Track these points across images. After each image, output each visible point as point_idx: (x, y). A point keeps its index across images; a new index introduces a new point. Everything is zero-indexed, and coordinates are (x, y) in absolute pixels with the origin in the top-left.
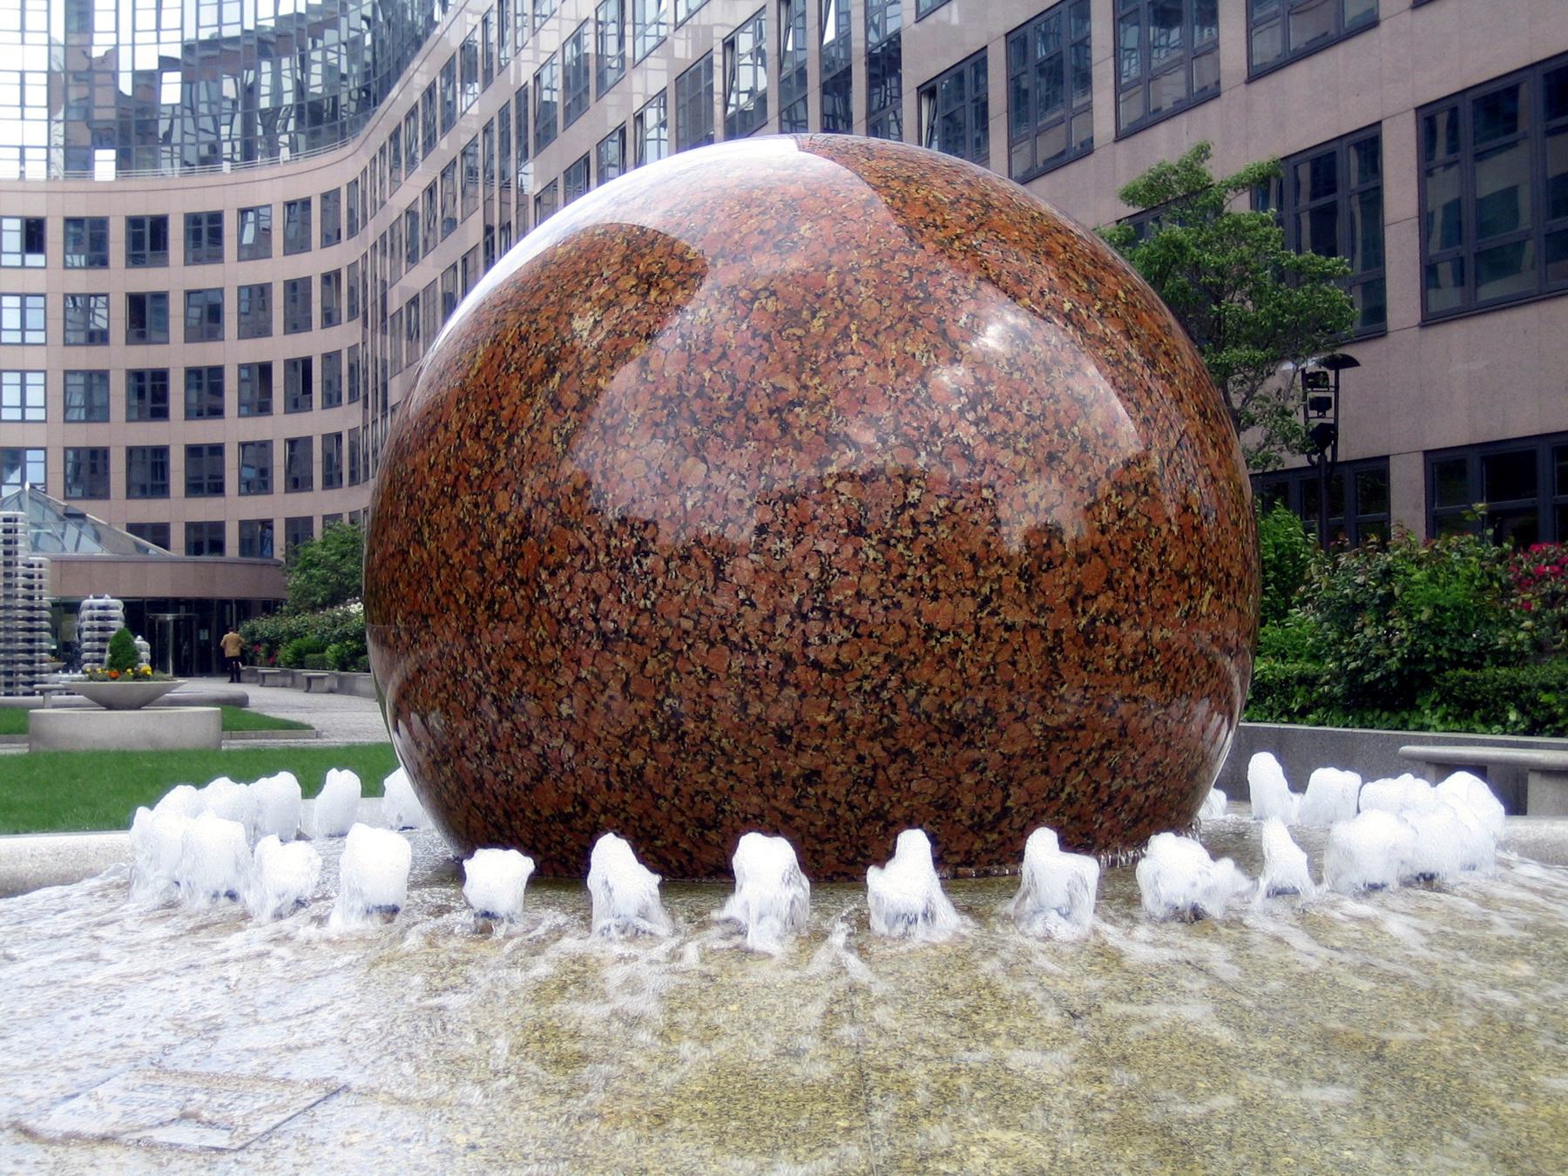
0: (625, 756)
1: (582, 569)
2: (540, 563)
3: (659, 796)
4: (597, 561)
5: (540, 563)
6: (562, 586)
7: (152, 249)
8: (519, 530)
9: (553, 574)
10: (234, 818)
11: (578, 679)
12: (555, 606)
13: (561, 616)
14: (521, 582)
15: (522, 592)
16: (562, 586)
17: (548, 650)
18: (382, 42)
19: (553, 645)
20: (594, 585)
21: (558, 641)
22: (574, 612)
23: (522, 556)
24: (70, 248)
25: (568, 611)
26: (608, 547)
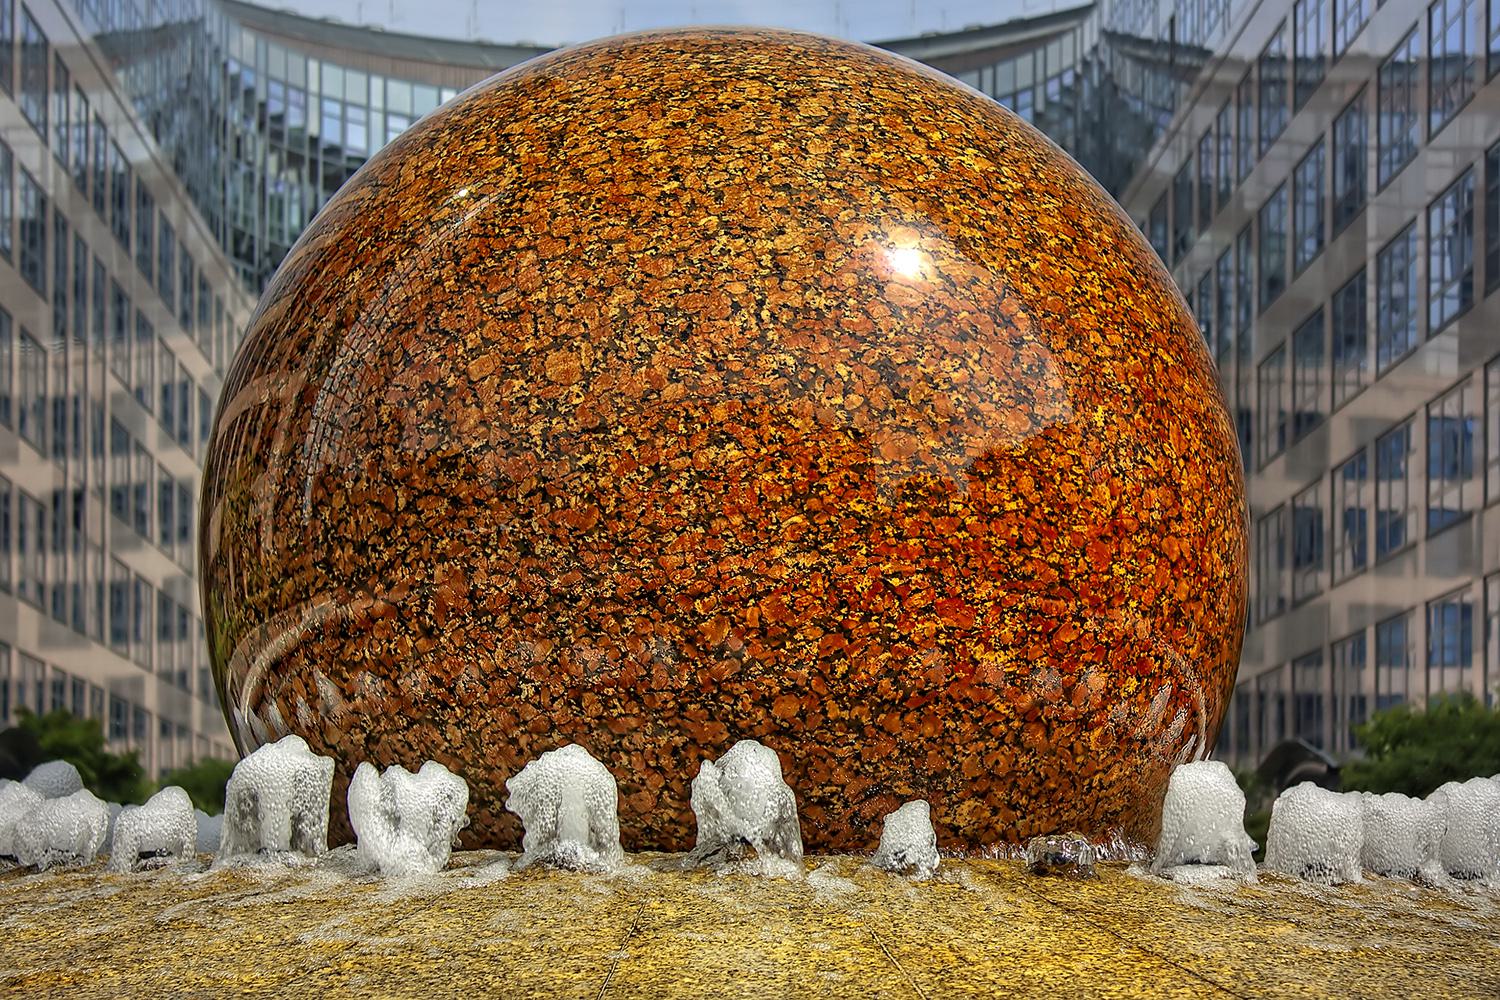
0: (459, 724)
1: (666, 787)
2: (693, 741)
3: (410, 724)
4: (668, 806)
5: (693, 741)
6: (657, 758)
7: (1363, 512)
8: (742, 724)
9: (675, 751)
10: (15, 844)
11: (553, 727)
12: (638, 738)
13: (625, 742)
14: (683, 707)
15: (671, 704)
16: (657, 758)
17: (596, 709)
18: (217, 143)
19: (599, 718)
20: (644, 794)
21: (600, 726)
22: (625, 759)
23: (712, 718)
24: (1476, 428)
25: (628, 752)
26: (680, 824)
